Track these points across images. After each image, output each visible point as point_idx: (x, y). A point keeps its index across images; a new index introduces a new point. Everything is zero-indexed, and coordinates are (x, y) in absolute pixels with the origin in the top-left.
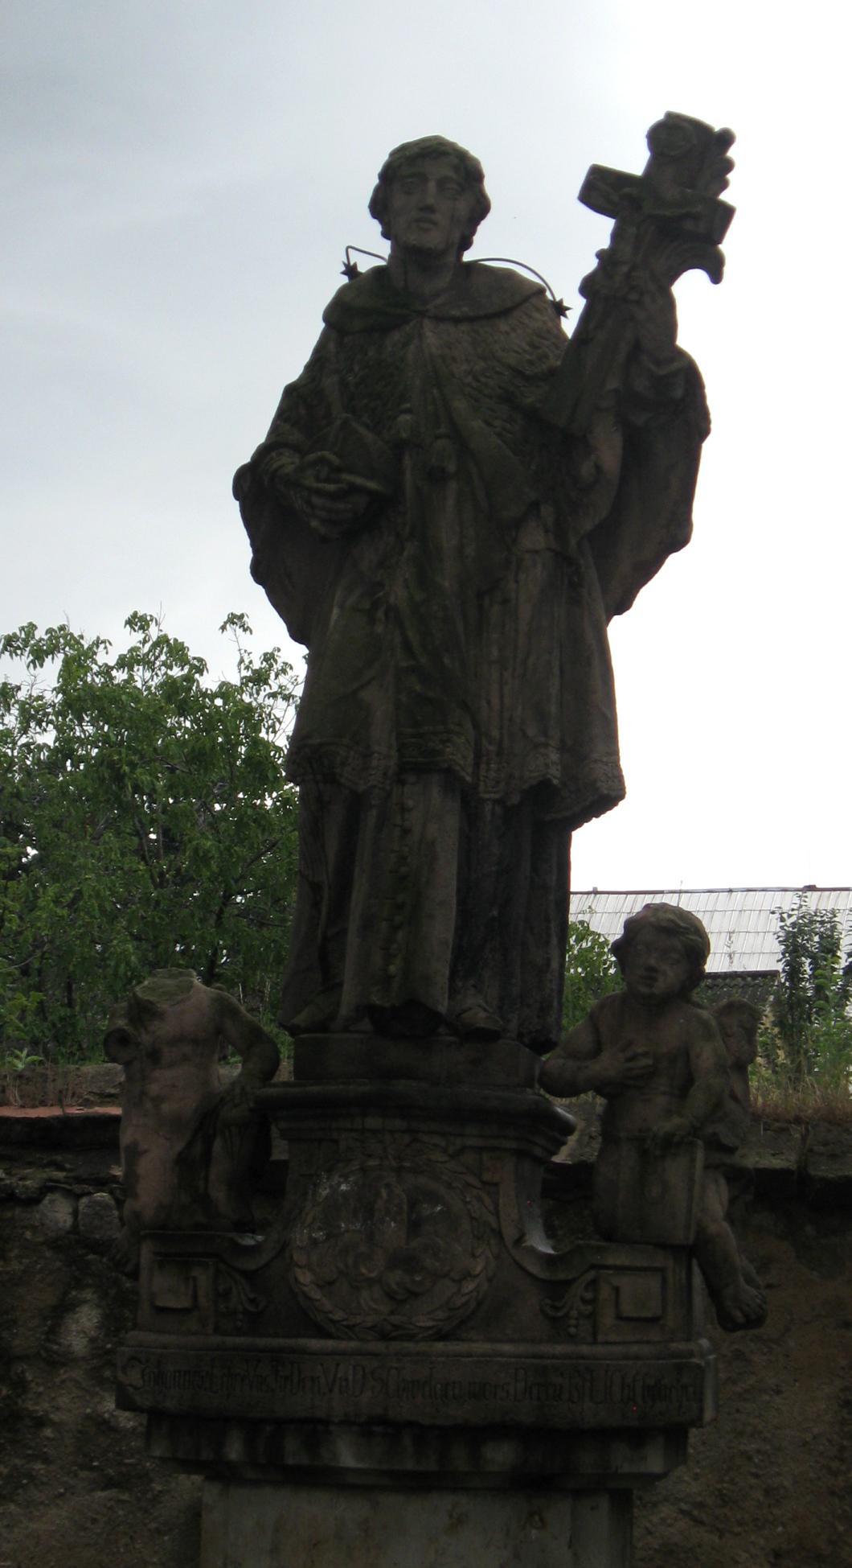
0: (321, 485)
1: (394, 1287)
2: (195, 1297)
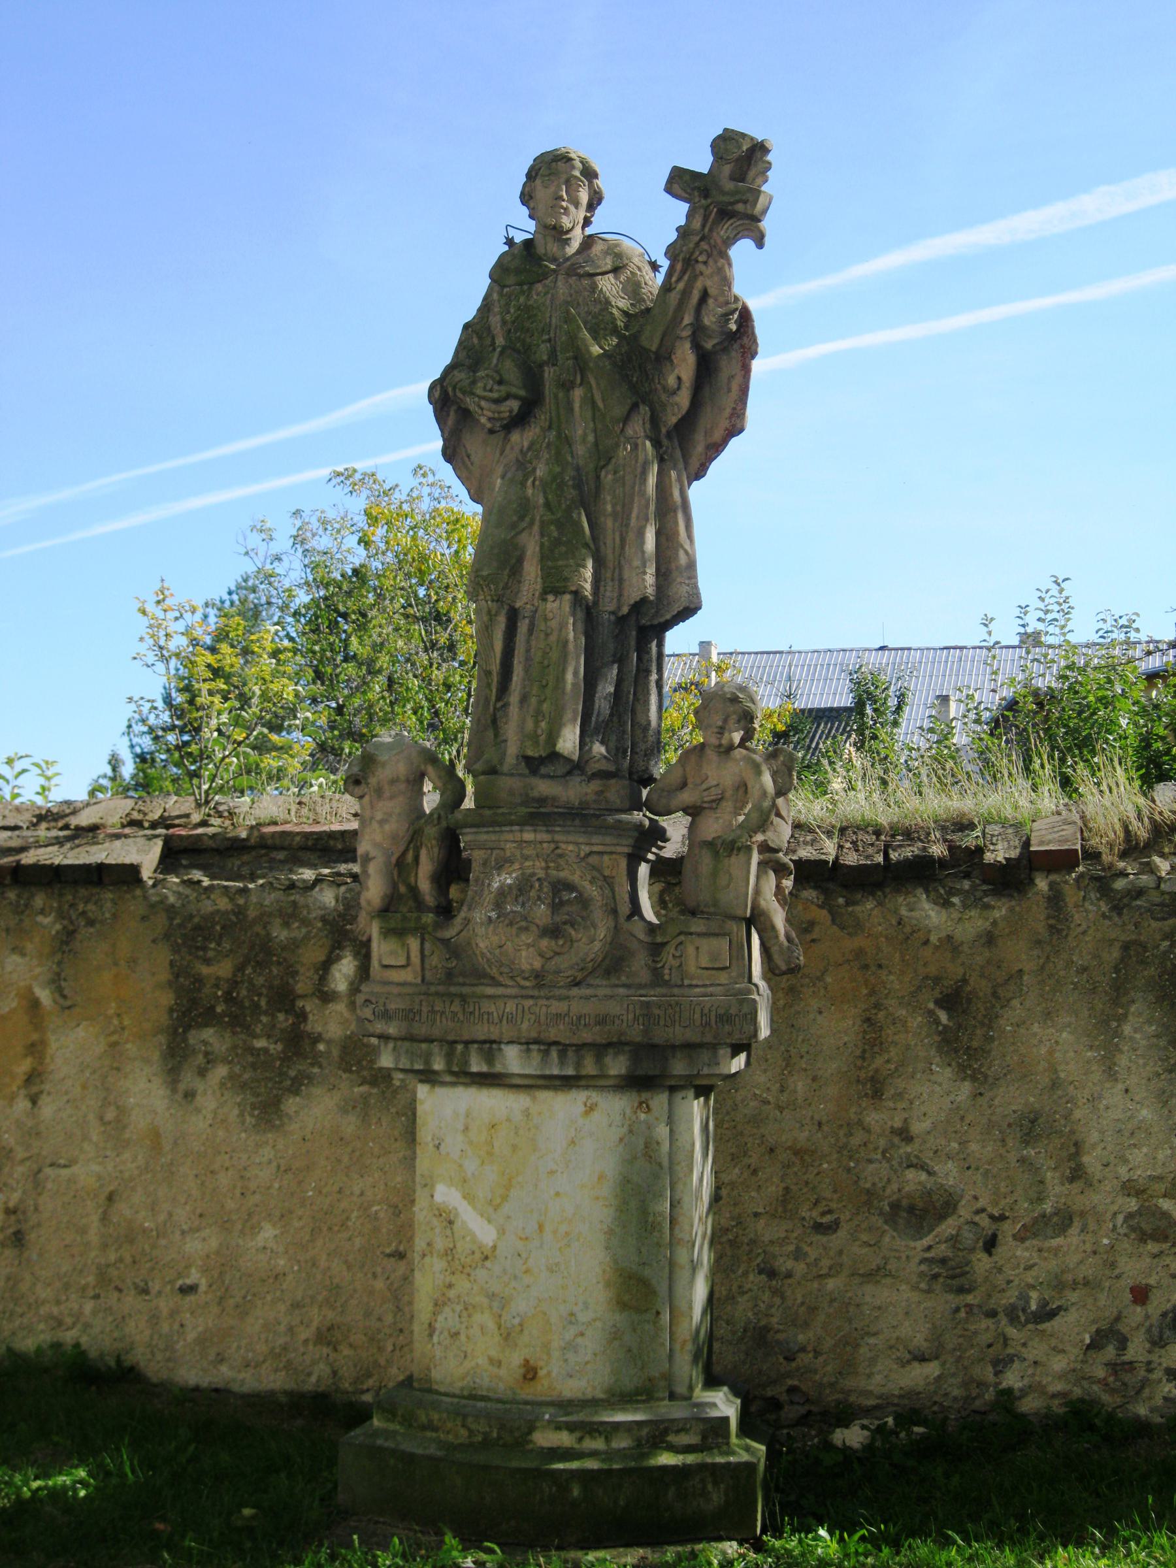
0: (486, 394)
2: (408, 958)
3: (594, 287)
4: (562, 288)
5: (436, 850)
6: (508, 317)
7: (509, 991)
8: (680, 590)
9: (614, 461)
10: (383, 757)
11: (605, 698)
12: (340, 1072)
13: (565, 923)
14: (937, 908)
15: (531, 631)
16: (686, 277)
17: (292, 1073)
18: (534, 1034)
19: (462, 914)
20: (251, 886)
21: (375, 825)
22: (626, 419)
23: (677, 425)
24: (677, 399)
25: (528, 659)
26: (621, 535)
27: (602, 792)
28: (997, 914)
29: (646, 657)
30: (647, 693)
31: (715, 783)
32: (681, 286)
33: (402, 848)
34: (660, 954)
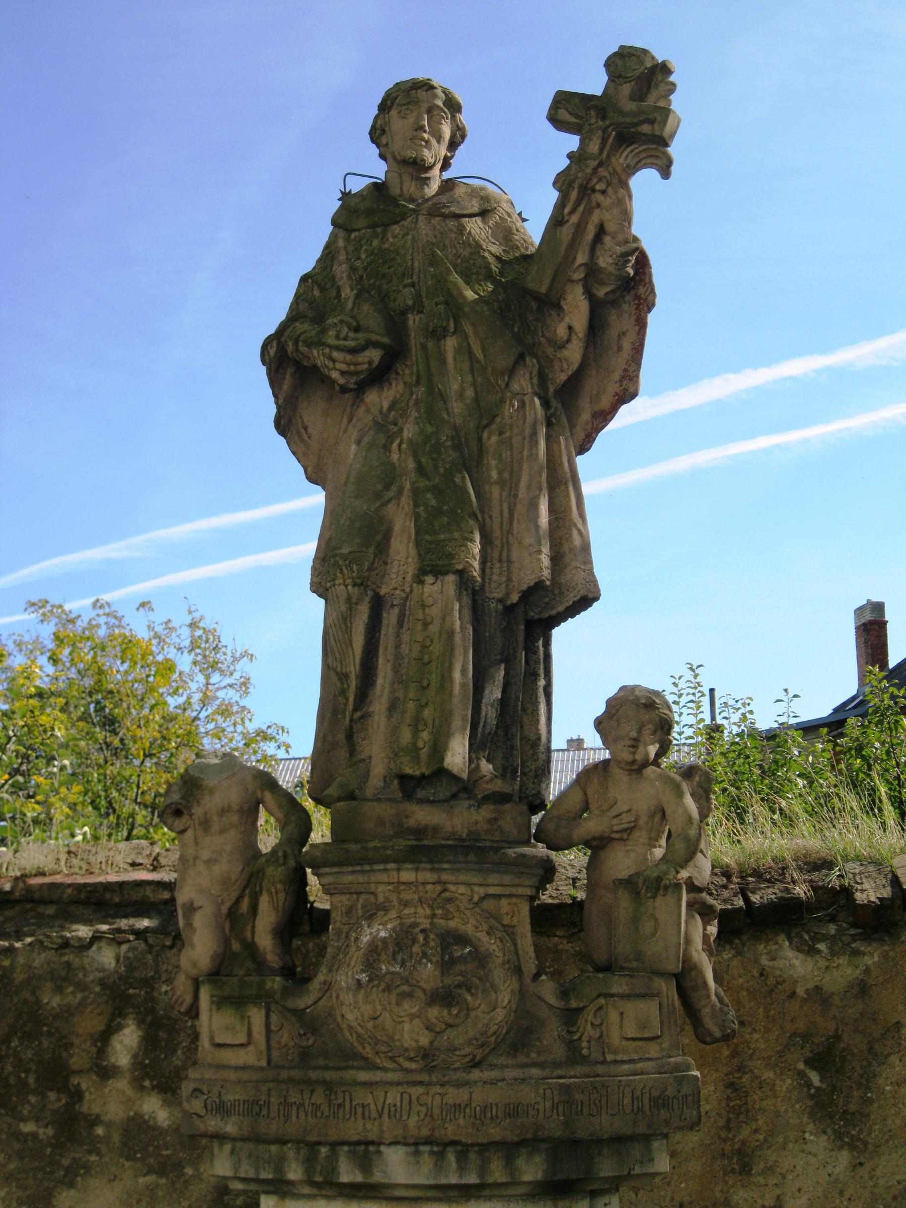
0: (341, 343)
1: (434, 1020)
2: (249, 1034)
3: (461, 229)
4: (425, 229)
5: (282, 896)
6: (358, 263)
7: (389, 1076)
8: (573, 575)
9: (498, 420)
10: (210, 781)
11: (492, 706)
12: (122, 1160)
13: (459, 986)
14: (801, 956)
15: (400, 624)
16: (581, 209)
17: (66, 1162)
18: (425, 1132)
19: (321, 977)
20: (18, 945)
21: (201, 867)
22: (512, 372)
23: (565, 384)
24: (565, 353)
25: (398, 656)
26: (509, 506)
27: (496, 819)
28: (868, 960)
29: (534, 657)
30: (536, 703)
31: (626, 808)
32: (575, 218)
33: (235, 895)
34: (575, 1024)
